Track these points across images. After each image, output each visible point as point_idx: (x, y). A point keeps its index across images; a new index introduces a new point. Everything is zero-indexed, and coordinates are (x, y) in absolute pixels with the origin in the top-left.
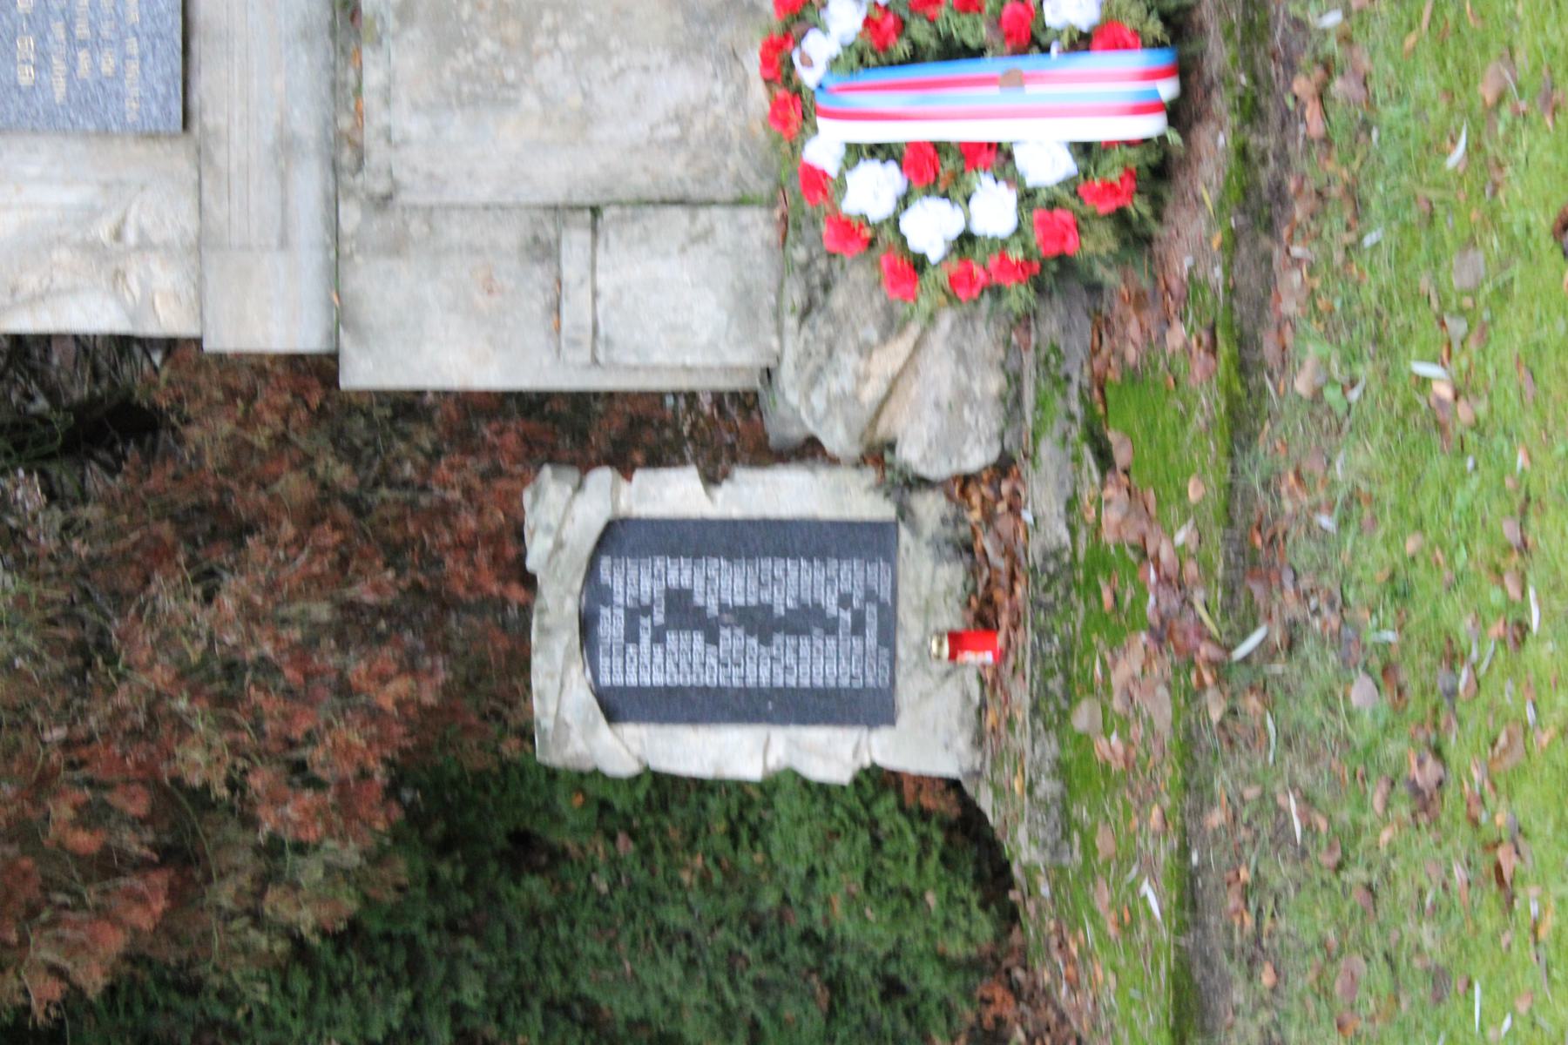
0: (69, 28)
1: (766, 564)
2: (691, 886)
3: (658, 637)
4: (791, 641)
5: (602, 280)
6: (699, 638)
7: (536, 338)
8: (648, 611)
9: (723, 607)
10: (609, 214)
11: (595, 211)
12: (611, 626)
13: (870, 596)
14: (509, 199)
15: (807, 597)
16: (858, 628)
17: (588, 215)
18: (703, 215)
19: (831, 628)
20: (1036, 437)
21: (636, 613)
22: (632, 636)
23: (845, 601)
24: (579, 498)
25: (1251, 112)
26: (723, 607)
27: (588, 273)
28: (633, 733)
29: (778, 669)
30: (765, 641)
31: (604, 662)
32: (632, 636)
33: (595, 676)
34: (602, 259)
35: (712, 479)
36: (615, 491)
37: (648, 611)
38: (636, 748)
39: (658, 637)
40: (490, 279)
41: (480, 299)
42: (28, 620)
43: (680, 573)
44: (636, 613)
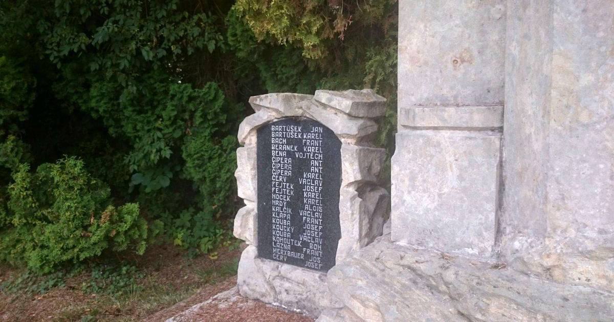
1: (320, 209)
2: (35, 232)
3: (290, 154)
4: (289, 217)
5: (446, 134)
6: (290, 174)
7: (424, 92)
8: (300, 150)
9: (303, 186)
10: (495, 139)
11: (501, 129)
12: (294, 132)
13: (308, 257)
14: (508, 68)
15: (307, 226)
16: (294, 248)
17: (497, 125)
18: (491, 207)
19: (295, 236)
21: (300, 144)
22: (290, 142)
23: (305, 244)
24: (346, 117)
26: (303, 186)
27: (452, 124)
28: (253, 140)
29: (278, 209)
30: (289, 205)
31: (280, 128)
32: (290, 142)
33: (275, 124)
34: (459, 134)
35: (240, 203)
36: (349, 136)
37: (300, 150)
38: (247, 142)
39: (290, 154)
40: (463, 61)
41: (450, 57)
42: (17, 230)
43: (316, 166)
44: (300, 144)
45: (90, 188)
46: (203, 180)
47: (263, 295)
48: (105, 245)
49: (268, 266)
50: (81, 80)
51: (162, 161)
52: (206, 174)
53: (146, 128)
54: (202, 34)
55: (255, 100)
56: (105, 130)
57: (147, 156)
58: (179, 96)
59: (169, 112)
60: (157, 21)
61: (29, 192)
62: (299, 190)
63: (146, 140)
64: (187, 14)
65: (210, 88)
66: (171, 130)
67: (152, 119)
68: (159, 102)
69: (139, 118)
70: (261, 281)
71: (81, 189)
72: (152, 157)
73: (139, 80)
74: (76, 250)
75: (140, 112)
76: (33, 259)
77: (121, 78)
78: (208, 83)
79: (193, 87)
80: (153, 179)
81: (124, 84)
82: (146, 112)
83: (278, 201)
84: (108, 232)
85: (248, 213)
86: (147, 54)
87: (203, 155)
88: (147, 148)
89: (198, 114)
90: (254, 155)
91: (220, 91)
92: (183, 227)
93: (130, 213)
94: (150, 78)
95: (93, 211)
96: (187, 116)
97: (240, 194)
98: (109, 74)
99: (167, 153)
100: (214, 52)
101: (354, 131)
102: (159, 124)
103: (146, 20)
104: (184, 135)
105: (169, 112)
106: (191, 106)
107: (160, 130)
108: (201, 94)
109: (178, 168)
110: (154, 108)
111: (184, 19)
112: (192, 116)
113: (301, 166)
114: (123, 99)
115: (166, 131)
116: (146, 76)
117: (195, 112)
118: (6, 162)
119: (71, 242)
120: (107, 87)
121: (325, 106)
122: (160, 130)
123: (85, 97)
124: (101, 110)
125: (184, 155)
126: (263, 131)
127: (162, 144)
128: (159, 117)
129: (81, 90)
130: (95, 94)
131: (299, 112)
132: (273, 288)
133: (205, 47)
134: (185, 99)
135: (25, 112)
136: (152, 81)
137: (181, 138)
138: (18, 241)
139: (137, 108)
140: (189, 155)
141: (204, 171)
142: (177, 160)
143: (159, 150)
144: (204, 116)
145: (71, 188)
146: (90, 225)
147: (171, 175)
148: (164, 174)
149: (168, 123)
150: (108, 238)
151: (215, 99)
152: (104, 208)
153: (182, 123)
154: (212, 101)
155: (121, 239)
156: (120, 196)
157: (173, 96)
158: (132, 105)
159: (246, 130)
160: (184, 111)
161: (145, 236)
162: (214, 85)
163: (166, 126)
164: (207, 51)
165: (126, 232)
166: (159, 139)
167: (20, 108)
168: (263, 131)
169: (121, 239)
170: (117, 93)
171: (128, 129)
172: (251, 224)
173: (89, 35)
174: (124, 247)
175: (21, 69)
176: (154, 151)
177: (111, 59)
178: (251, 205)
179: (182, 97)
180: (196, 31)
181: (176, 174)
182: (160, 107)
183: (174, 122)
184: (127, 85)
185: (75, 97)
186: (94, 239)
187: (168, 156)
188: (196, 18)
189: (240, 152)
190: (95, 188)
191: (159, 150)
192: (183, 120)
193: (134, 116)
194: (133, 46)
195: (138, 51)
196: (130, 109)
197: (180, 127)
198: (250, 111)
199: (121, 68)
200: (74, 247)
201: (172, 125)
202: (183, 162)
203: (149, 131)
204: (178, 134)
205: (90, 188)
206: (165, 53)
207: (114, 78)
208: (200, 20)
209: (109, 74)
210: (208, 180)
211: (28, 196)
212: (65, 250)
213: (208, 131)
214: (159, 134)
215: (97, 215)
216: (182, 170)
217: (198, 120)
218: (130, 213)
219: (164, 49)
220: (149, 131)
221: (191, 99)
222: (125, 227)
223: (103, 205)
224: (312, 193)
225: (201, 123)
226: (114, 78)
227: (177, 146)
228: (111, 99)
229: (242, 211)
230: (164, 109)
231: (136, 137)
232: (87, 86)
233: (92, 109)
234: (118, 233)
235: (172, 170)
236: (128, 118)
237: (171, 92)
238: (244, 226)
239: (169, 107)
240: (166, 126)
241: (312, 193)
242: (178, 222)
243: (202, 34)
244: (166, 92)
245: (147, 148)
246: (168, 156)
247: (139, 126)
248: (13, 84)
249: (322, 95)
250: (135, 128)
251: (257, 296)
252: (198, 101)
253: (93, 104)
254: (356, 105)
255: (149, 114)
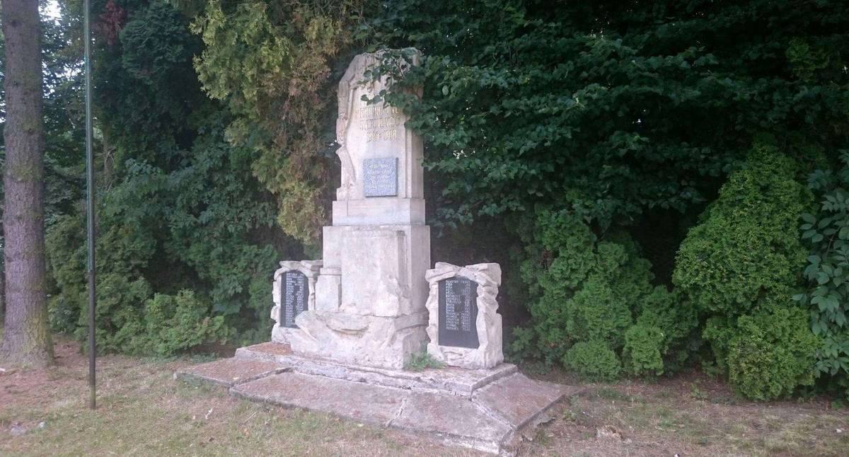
0: (379, 174)
3: (293, 284)
10: (339, 277)
12: (294, 275)
20: (123, 399)
22: (293, 279)
25: (430, 385)
28: (280, 278)
32: (293, 279)
45: (196, 307)
46: (262, 308)
47: (281, 341)
48: (204, 338)
49: (283, 329)
50: (185, 241)
51: (236, 295)
52: (264, 303)
53: (226, 273)
54: (265, 216)
55: (282, 263)
56: (196, 274)
57: (225, 291)
58: (249, 253)
59: (242, 263)
60: (237, 208)
61: (160, 310)
62: (296, 298)
63: (226, 281)
64: (256, 203)
65: (268, 248)
66: (242, 275)
67: (230, 267)
68: (235, 256)
69: (222, 267)
70: (280, 335)
71: (192, 307)
72: (229, 292)
73: (224, 243)
74: (187, 341)
75: (223, 263)
76: (161, 348)
77: (214, 242)
78: (268, 246)
79: (259, 248)
80: (228, 308)
81: (215, 246)
82: (227, 263)
83: (289, 302)
84: (207, 330)
85: (276, 308)
86: (231, 229)
87: (262, 291)
88: (226, 286)
89: (261, 265)
90: (280, 285)
91: (275, 251)
92: (247, 339)
93: (219, 321)
94: (231, 241)
95: (462, 86)
96: (253, 266)
97: (274, 301)
98: (206, 239)
99: (240, 290)
100: (272, 227)
101: (312, 275)
102: (235, 270)
103: (231, 207)
104: (251, 278)
105: (242, 263)
106: (256, 260)
107: (235, 274)
108: (263, 252)
109: (245, 301)
110: (232, 260)
111: (254, 206)
112: (256, 266)
113: (296, 289)
114: (213, 254)
115: (239, 275)
116: (229, 240)
117: (259, 263)
118: (138, 293)
119: (185, 336)
120: (203, 247)
121: (304, 267)
122: (235, 274)
123: (185, 252)
124: (197, 261)
125: (250, 292)
126: (284, 275)
127: (237, 284)
128: (235, 266)
129: (184, 247)
130: (194, 251)
131: (296, 269)
132: (285, 337)
133: (267, 224)
134: (253, 255)
135: (147, 262)
136: (232, 243)
137: (249, 281)
138: (149, 340)
139: (222, 260)
140: (254, 291)
141: (263, 301)
142: (245, 295)
143: (235, 288)
144: (264, 266)
145: (186, 306)
146: (196, 327)
147: (240, 305)
148: (235, 304)
149: (241, 270)
150: (206, 334)
151: (272, 255)
152: (204, 318)
153: (250, 270)
154: (269, 257)
155: (213, 335)
156: (211, 312)
157: (245, 253)
158: (218, 258)
159: (277, 276)
160: (252, 263)
161: (226, 335)
162: (271, 246)
163: (240, 272)
164: (268, 227)
165: (216, 332)
166: (234, 280)
167: (143, 259)
168: (284, 275)
169: (213, 335)
170: (208, 251)
171: (213, 274)
172: (278, 312)
173: (197, 216)
174: (214, 341)
175: (147, 234)
176: (231, 288)
177: (208, 230)
178: (279, 305)
179: (251, 254)
180: (262, 213)
181: (244, 306)
182: (236, 260)
183: (244, 270)
184: (217, 247)
185: (179, 252)
186: (199, 334)
187: (240, 292)
188: (262, 205)
189: (274, 283)
190: (199, 306)
191: (235, 288)
192: (251, 268)
193: (219, 265)
194: (222, 224)
195: (225, 226)
196: (217, 261)
197: (248, 273)
198: (280, 267)
199: (142, 155)
200: (186, 339)
201: (243, 271)
202: (249, 296)
203: (228, 275)
204: (247, 277)
205: (198, 307)
206: (242, 227)
207: (209, 242)
208: (264, 207)
209: (206, 239)
210: (265, 307)
211: (159, 312)
212: (181, 342)
213: (267, 275)
214: (235, 277)
215: (200, 322)
216: (247, 302)
217: (260, 269)
218: (219, 321)
219: (242, 225)
220: (228, 275)
221: (257, 255)
222: (216, 328)
223: (203, 317)
224: (300, 299)
225: (262, 271)
226: (209, 242)
227: (246, 284)
228: (204, 254)
229: (274, 307)
230: (239, 261)
231: (218, 279)
232: (188, 245)
233: (190, 260)
234: (212, 331)
235: (241, 301)
236: (215, 267)
237: (244, 251)
238: (275, 314)
239: (242, 259)
240: (240, 272)
241: (300, 299)
242: (244, 335)
243: (265, 216)
244: (241, 250)
245: (226, 286)
246: (240, 292)
247: (222, 271)
248: (143, 244)
249: (303, 262)
250: (219, 273)
251: (279, 341)
252: (261, 256)
253: (192, 257)
254: (313, 266)
255: (229, 264)
